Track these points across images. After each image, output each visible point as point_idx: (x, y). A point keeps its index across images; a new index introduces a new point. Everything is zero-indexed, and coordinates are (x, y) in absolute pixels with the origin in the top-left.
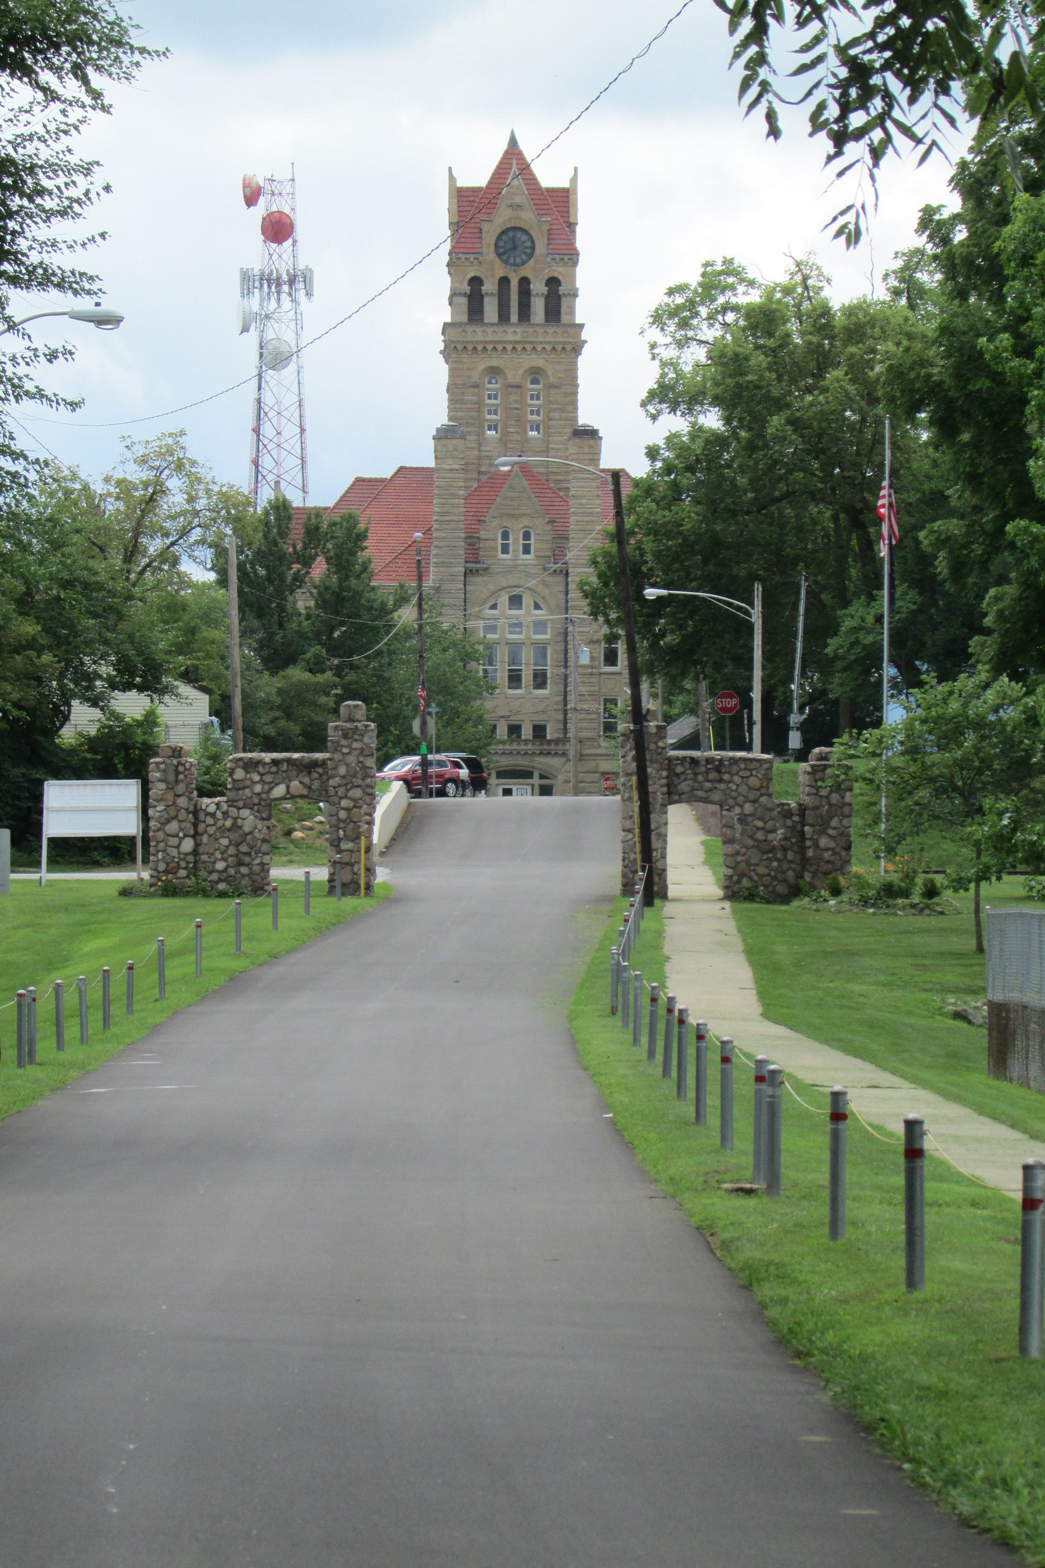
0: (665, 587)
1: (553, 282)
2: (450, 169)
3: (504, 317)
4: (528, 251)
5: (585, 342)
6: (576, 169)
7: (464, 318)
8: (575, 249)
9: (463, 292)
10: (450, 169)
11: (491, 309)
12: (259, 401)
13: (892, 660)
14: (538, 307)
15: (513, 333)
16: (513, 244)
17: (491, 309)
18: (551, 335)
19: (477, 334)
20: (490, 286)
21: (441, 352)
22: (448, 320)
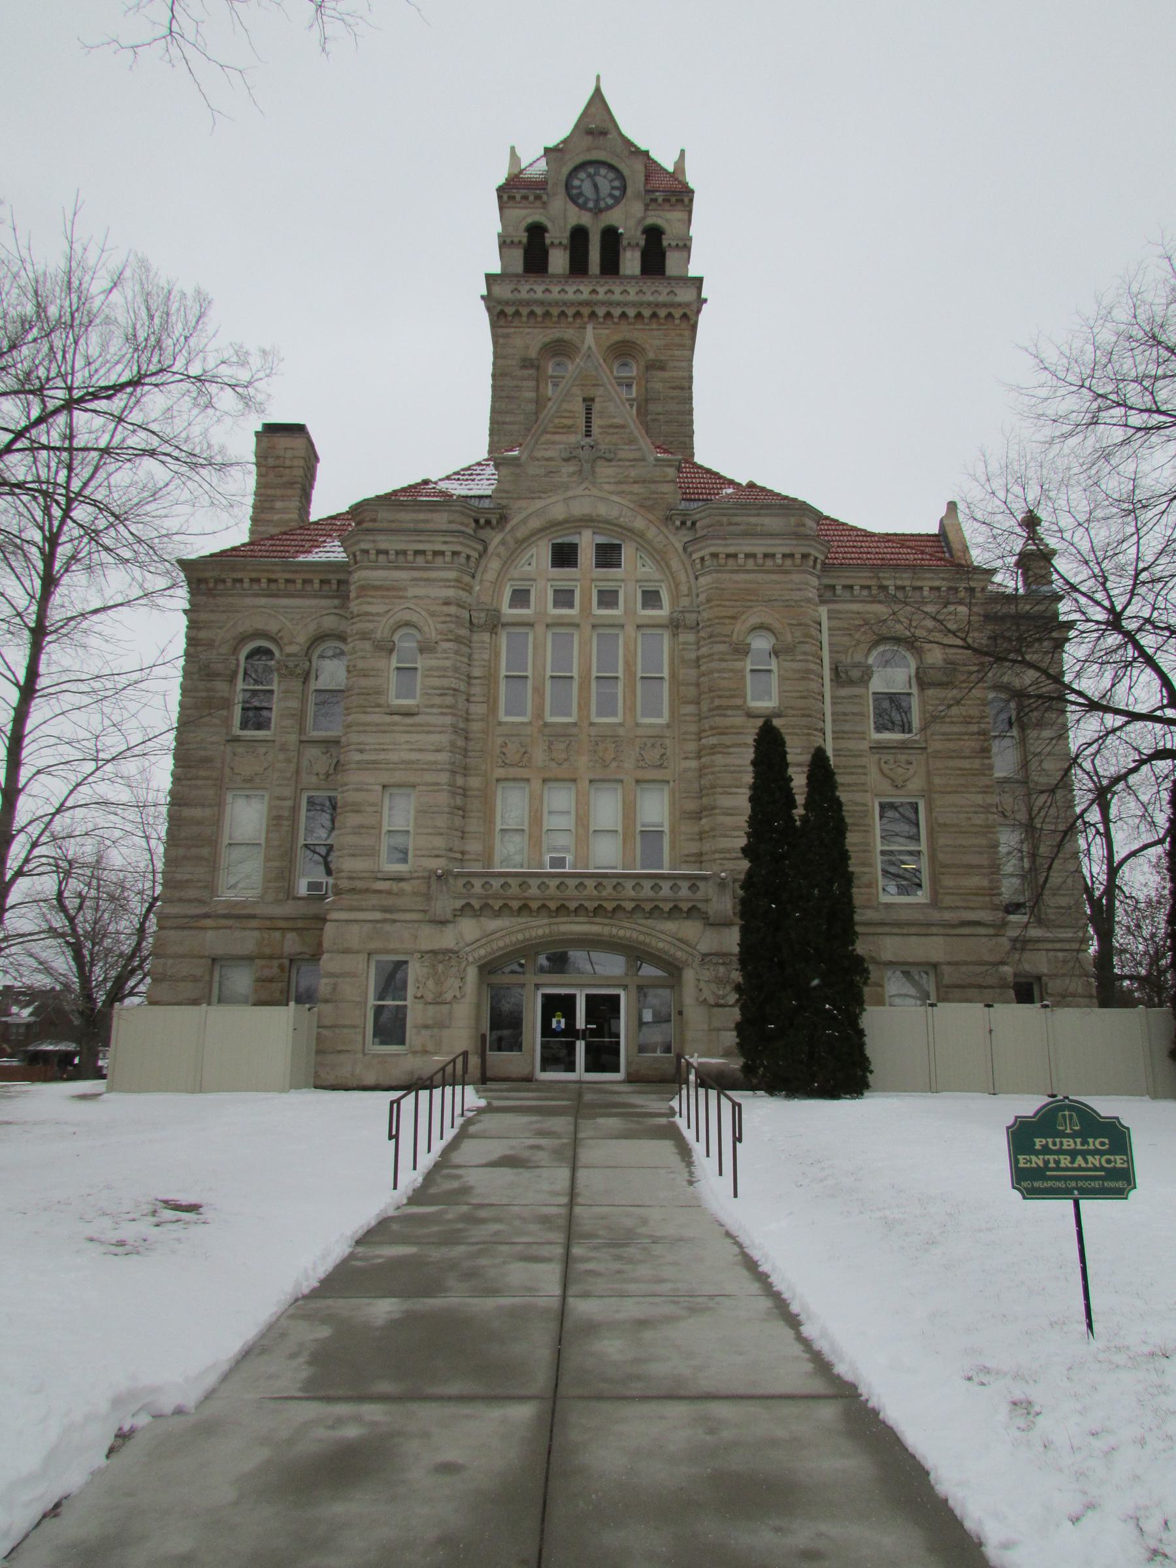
0: (723, 1056)
1: (654, 234)
2: (513, 148)
3: (578, 267)
4: (617, 193)
5: (705, 301)
6: (683, 152)
7: (519, 268)
8: (686, 185)
9: (516, 240)
10: (513, 148)
11: (558, 260)
12: (231, 464)
13: (409, 1320)
14: (631, 262)
15: (579, 291)
16: (592, 253)
17: (558, 260)
18: (655, 292)
19: (535, 290)
20: (558, 234)
21: (483, 297)
22: (497, 269)
